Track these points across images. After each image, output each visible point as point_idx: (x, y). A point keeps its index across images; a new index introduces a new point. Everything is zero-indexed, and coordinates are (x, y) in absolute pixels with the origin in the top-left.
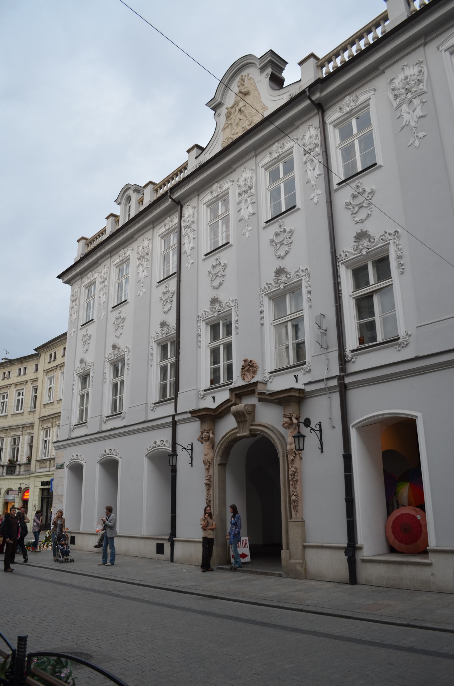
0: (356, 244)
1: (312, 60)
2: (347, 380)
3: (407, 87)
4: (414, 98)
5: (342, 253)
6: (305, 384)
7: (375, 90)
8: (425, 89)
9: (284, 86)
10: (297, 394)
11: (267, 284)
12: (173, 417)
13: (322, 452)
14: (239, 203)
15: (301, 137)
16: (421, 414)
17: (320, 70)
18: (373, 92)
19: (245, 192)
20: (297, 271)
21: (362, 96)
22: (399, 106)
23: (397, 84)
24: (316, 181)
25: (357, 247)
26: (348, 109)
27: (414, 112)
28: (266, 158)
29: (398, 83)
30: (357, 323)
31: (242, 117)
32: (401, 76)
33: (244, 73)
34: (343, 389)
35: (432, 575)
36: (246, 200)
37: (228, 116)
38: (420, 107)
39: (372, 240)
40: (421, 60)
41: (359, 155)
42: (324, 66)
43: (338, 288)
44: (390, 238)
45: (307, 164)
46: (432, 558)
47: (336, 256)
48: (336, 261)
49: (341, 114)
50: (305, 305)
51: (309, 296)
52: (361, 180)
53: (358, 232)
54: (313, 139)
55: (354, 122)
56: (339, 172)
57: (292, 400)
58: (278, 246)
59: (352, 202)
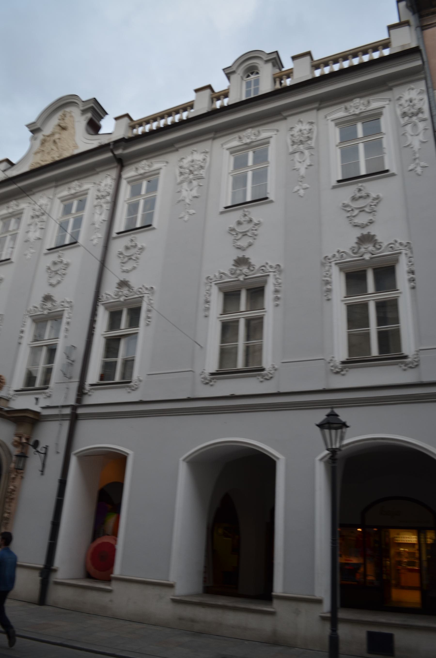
1: (126, 119)
2: (80, 411)
3: (191, 168)
6: (43, 408)
10: (31, 416)
12: (74, 408)
13: (42, 474)
14: (30, 225)
19: (38, 216)
20: (63, 302)
22: (182, 182)
26: (248, 141)
28: (64, 192)
29: (186, 163)
31: (54, 147)
32: (189, 158)
33: (68, 109)
34: (74, 418)
36: (36, 224)
37: (43, 143)
40: (207, 150)
44: (401, 248)
49: (239, 144)
50: (62, 334)
52: (364, 184)
55: (251, 155)
56: (120, 225)
57: (28, 420)
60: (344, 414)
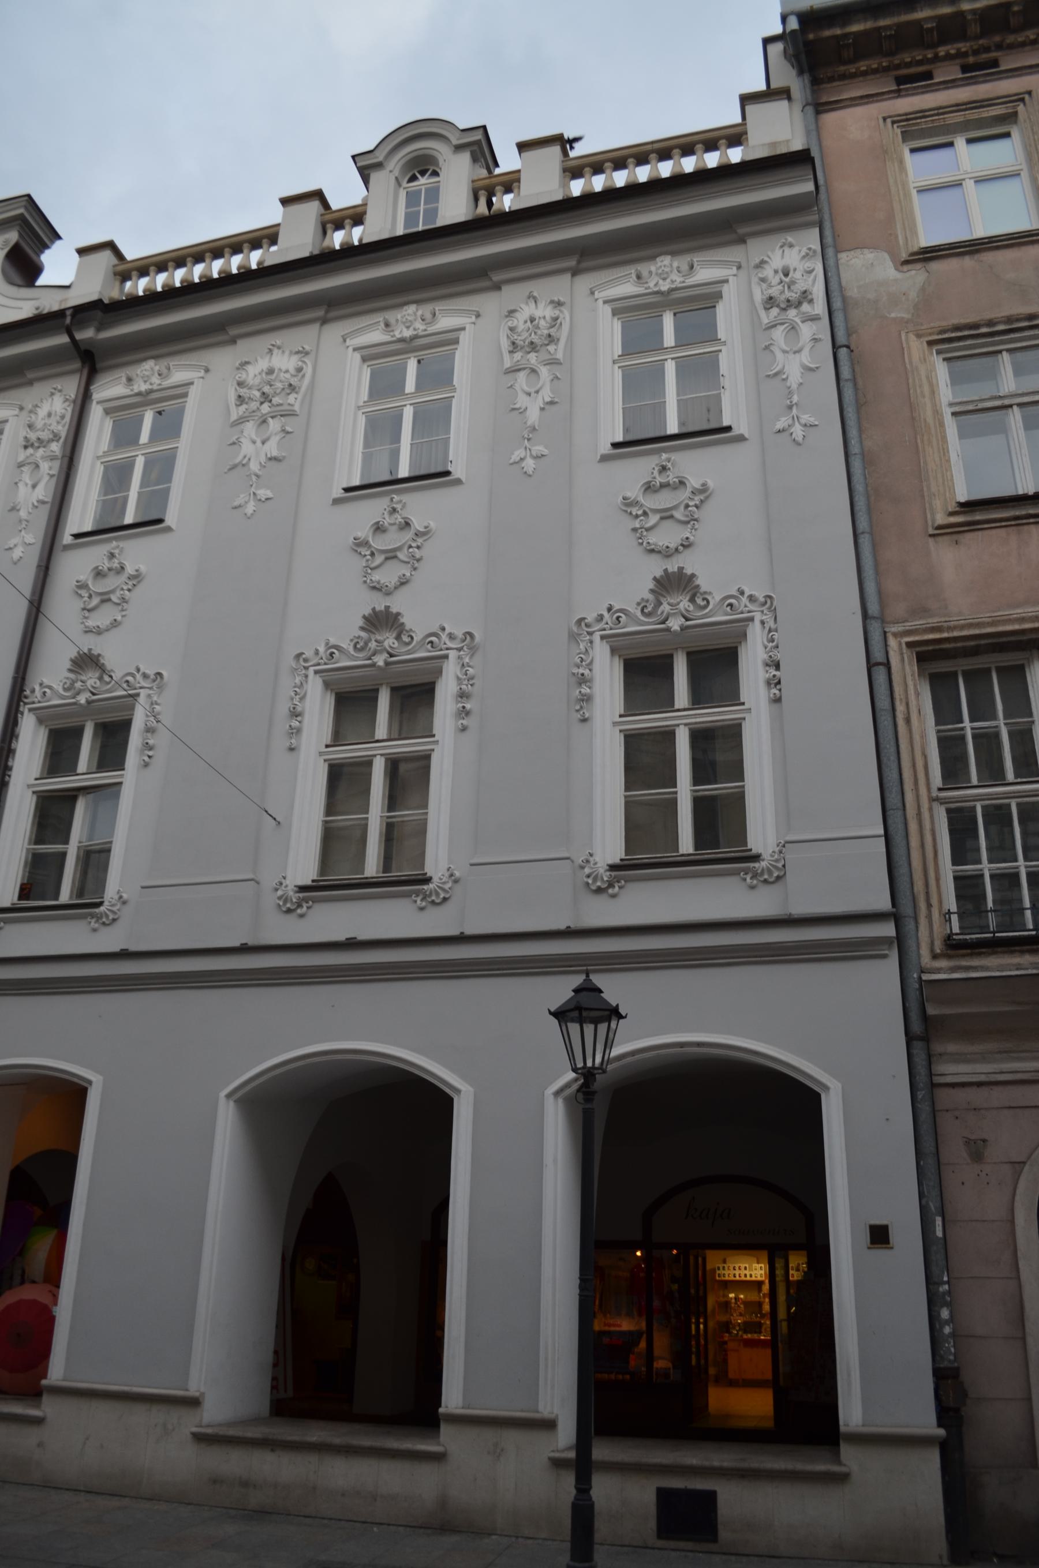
0: (72, 676)
1: (107, 255)
3: (266, 389)
4: (272, 417)
5: (37, 688)
7: (478, 316)
8: (297, 408)
9: (39, 283)
11: (609, 609)
15: (30, 406)
16: (101, 1078)
17: (117, 283)
18: (202, 373)
21: (180, 371)
22: (241, 421)
23: (251, 375)
24: (30, 513)
25: (74, 682)
26: (144, 387)
27: (263, 443)
29: (253, 374)
30: (28, 850)
32: (263, 364)
35: (40, 1445)
38: (278, 438)
39: (406, 639)
40: (307, 348)
41: (409, 441)
42: (129, 278)
43: (7, 760)
44: (450, 645)
45: (25, 469)
46: (49, 1408)
47: (22, 690)
48: (19, 700)
49: (386, 338)
51: (773, 672)
53: (378, 609)
54: (53, 421)
55: (148, 418)
56: (82, 515)
58: (95, 601)
59: (90, 583)
60: (614, 988)
